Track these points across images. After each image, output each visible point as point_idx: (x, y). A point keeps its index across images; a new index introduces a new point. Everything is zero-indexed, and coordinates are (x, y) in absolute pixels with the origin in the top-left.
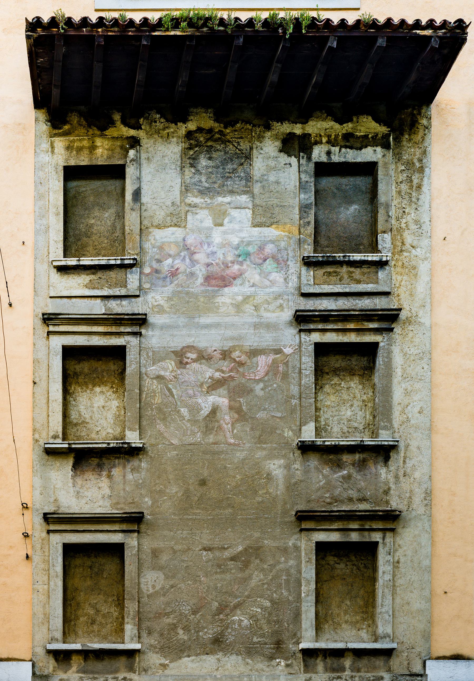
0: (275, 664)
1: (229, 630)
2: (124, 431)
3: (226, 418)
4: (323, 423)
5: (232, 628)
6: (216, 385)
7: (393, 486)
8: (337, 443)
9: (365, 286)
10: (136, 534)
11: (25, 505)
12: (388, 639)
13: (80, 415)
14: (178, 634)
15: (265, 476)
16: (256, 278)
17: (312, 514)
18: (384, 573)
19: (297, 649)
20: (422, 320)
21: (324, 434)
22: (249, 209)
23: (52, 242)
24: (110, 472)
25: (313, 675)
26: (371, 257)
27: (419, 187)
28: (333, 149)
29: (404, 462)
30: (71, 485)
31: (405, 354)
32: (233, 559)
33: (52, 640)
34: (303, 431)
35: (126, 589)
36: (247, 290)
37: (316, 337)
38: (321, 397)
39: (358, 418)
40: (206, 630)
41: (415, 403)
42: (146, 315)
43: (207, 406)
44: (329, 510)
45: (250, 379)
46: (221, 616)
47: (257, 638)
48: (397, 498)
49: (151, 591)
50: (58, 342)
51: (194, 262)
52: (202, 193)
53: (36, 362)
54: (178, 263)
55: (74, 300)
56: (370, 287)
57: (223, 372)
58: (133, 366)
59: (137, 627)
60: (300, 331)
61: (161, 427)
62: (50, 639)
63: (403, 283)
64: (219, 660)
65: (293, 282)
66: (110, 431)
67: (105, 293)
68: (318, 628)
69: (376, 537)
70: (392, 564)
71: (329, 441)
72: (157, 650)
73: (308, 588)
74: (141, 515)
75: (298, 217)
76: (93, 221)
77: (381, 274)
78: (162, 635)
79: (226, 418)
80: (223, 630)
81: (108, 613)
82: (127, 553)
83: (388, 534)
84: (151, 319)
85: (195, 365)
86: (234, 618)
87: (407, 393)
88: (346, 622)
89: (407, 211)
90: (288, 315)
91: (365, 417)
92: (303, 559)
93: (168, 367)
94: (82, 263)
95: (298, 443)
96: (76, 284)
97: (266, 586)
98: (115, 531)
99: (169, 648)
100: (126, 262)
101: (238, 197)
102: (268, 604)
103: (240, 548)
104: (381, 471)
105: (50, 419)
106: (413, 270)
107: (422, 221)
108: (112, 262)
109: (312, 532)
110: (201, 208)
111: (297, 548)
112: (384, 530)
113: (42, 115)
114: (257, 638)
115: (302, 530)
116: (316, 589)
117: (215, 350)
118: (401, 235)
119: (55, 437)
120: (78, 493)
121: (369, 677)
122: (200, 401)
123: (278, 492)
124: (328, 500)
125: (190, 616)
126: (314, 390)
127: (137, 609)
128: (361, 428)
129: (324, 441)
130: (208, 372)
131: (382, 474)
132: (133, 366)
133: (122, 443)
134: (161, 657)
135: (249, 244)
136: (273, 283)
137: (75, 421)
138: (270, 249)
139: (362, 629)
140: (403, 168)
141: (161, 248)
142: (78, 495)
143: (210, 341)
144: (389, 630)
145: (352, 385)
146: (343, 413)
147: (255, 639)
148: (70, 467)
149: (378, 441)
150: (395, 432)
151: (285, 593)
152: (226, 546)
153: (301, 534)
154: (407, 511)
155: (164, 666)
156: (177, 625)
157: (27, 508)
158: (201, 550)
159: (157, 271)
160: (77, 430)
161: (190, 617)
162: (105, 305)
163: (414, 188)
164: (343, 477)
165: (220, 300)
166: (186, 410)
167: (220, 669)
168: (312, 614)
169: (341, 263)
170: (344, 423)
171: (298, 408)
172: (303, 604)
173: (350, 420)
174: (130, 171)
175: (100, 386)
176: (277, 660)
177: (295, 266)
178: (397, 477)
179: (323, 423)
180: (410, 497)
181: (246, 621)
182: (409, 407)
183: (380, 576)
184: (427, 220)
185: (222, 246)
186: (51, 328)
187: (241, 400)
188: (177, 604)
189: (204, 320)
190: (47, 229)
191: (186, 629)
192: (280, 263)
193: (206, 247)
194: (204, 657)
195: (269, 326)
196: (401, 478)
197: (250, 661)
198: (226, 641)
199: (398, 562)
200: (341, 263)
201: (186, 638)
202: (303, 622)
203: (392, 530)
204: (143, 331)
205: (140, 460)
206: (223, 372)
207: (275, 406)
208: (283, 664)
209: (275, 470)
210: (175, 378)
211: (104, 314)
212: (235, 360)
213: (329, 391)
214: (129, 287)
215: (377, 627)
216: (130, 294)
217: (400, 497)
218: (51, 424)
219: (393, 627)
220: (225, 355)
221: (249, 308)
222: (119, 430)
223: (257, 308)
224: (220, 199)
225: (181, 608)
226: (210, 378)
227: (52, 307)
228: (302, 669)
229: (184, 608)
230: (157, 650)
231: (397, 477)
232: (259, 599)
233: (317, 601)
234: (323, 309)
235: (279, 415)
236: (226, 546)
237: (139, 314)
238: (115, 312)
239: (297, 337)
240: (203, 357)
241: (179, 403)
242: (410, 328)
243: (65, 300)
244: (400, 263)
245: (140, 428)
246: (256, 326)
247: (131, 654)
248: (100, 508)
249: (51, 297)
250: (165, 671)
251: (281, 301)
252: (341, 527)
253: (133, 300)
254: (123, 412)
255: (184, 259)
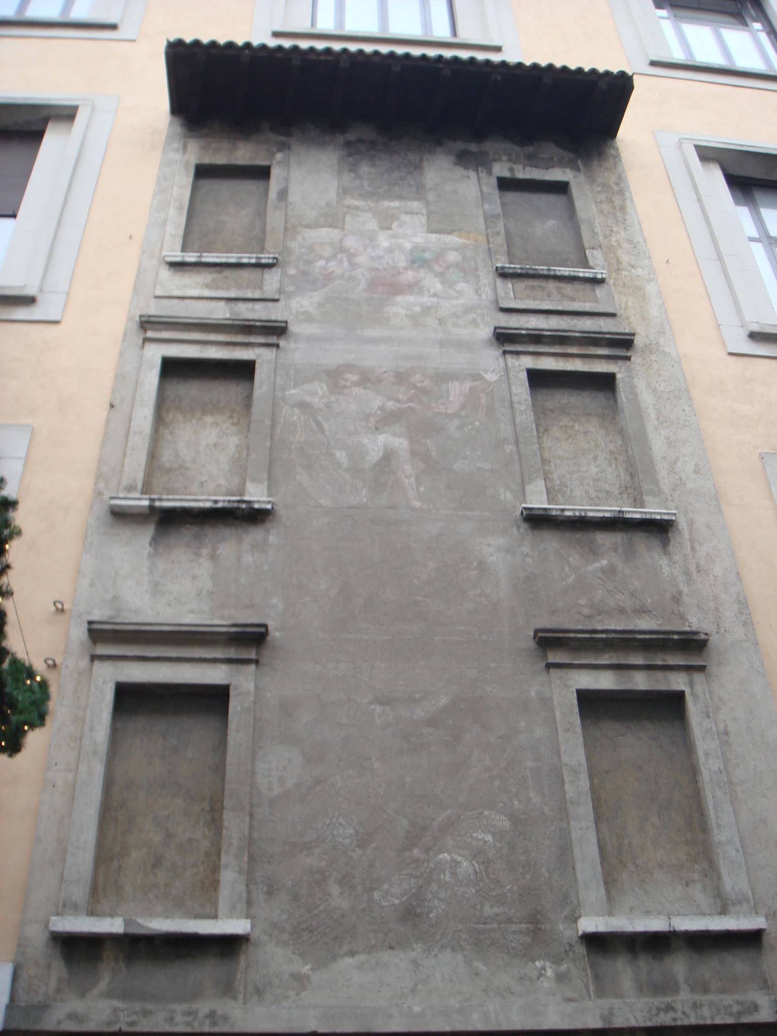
0: (535, 974)
1: (434, 887)
2: (244, 483)
3: (407, 470)
4: (557, 482)
5: (439, 880)
6: (386, 420)
7: (685, 590)
8: (583, 514)
9: (581, 304)
10: (252, 667)
11: (59, 606)
12: (745, 905)
13: (177, 456)
14: (330, 895)
15: (475, 564)
16: (438, 287)
17: (561, 635)
18: (707, 754)
19: (574, 934)
20: (667, 350)
21: (561, 499)
22: (423, 214)
23: (167, 236)
24: (214, 549)
25: (615, 1001)
26: (582, 273)
27: (623, 208)
28: (516, 167)
29: (693, 548)
30: (145, 570)
31: (655, 391)
32: (432, 722)
33: (64, 906)
34: (528, 493)
35: (228, 786)
36: (426, 300)
37: (529, 362)
38: (547, 443)
39: (609, 477)
40: (386, 886)
41: (686, 459)
42: (286, 322)
43: (376, 448)
44: (590, 628)
45: (439, 413)
46: (416, 852)
47: (491, 907)
48: (696, 609)
49: (277, 790)
50: (156, 354)
51: (354, 266)
52: (363, 196)
53: (120, 377)
54: (332, 266)
55: (187, 301)
56: (588, 307)
57: (398, 401)
58: (265, 388)
59: (244, 877)
60: (505, 352)
61: (303, 477)
62: (61, 904)
63: (630, 304)
64: (415, 963)
65: (487, 294)
66: (222, 482)
67: (232, 295)
68: (610, 882)
69: (677, 682)
70: (716, 737)
71: (570, 510)
72: (286, 936)
73: (578, 786)
74: (262, 630)
75: (484, 226)
76: (226, 218)
77: (600, 292)
78: (296, 897)
79: (407, 470)
80: (421, 887)
81: (190, 840)
82: (235, 705)
83: (698, 677)
84: (293, 328)
85: (355, 390)
86: (441, 856)
87: (670, 443)
88: (661, 865)
89: (615, 229)
90: (485, 332)
91: (618, 476)
92: (559, 724)
93: (317, 392)
94: (204, 260)
95: (522, 512)
96: (192, 284)
97: (497, 783)
98: (214, 661)
99: (312, 932)
100: (263, 261)
101: (409, 203)
102: (503, 823)
103: (443, 701)
104: (661, 562)
105: (127, 461)
106: (639, 291)
107: (635, 241)
108: (245, 261)
109: (568, 670)
110: (363, 211)
111: (546, 703)
112: (688, 668)
113: (178, 122)
114: (491, 907)
115: (549, 666)
116: (592, 788)
117: (385, 372)
118: (615, 254)
119: (130, 488)
120: (156, 584)
121: (730, 1006)
122: (365, 441)
123: (501, 594)
124: (586, 611)
125: (354, 851)
126: (535, 433)
127: (246, 833)
128: (616, 492)
129: (563, 510)
130: (376, 402)
131: (664, 566)
132: (265, 388)
133: (239, 502)
134: (293, 956)
135: (424, 250)
136: (460, 294)
137: (167, 465)
138: (452, 257)
139: (693, 881)
140: (599, 189)
141: (311, 249)
142: (156, 589)
143: (379, 357)
144: (743, 885)
145: (591, 429)
146: (584, 469)
147: (488, 911)
148: (148, 539)
149: (645, 513)
150: (667, 499)
151: (535, 798)
152: (417, 696)
153: (548, 673)
154: (717, 633)
155: (300, 980)
156: (327, 874)
157: (63, 610)
158: (371, 703)
159: (305, 273)
160: (170, 479)
161: (353, 854)
162: (231, 309)
163: (617, 208)
164: (602, 570)
165: (391, 310)
166: (344, 453)
167: (419, 987)
168: (592, 849)
169: (546, 277)
170: (589, 484)
171: (516, 458)
172: (572, 823)
173: (596, 480)
174: (275, 172)
175: (212, 415)
176: (538, 964)
177: (486, 277)
178: (687, 573)
179: (557, 482)
180: (717, 609)
181: (465, 864)
182: (679, 464)
183: (701, 763)
184: (641, 240)
185: (390, 250)
186: (150, 334)
187: (428, 442)
188: (328, 821)
189: (371, 333)
190: (165, 223)
191: (345, 881)
192: (466, 270)
193: (369, 250)
194: (386, 956)
195: (460, 345)
196: (694, 574)
197: (483, 968)
198: (428, 914)
199: (726, 733)
200: (546, 277)
201: (346, 905)
202: (579, 865)
203: (702, 669)
204: (282, 343)
205: (267, 532)
206: (398, 401)
207: (479, 453)
208: (549, 973)
209: (492, 555)
210: (327, 406)
211: (227, 319)
212: (414, 386)
213: (558, 436)
214: (265, 288)
215: (719, 877)
216: (266, 296)
217: (700, 608)
218: (126, 468)
219: (749, 875)
220: (401, 378)
221: (431, 321)
222: (236, 480)
223: (441, 321)
224: (386, 203)
225: (335, 833)
226: (380, 408)
227: (154, 309)
228: (592, 987)
229: (341, 831)
230: (286, 936)
231: (687, 573)
232: (486, 813)
233: (598, 819)
234: (530, 327)
235: (488, 466)
236: (417, 696)
237: (276, 321)
238: (242, 317)
239: (501, 361)
240: (367, 379)
241: (332, 443)
242: (653, 357)
243: (176, 301)
244: (621, 283)
245: (269, 478)
246: (443, 344)
247: (229, 945)
248: (191, 615)
249: (156, 297)
250: (303, 994)
251: (474, 316)
252: (615, 661)
253: (270, 304)
254: (245, 454)
255: (341, 261)
